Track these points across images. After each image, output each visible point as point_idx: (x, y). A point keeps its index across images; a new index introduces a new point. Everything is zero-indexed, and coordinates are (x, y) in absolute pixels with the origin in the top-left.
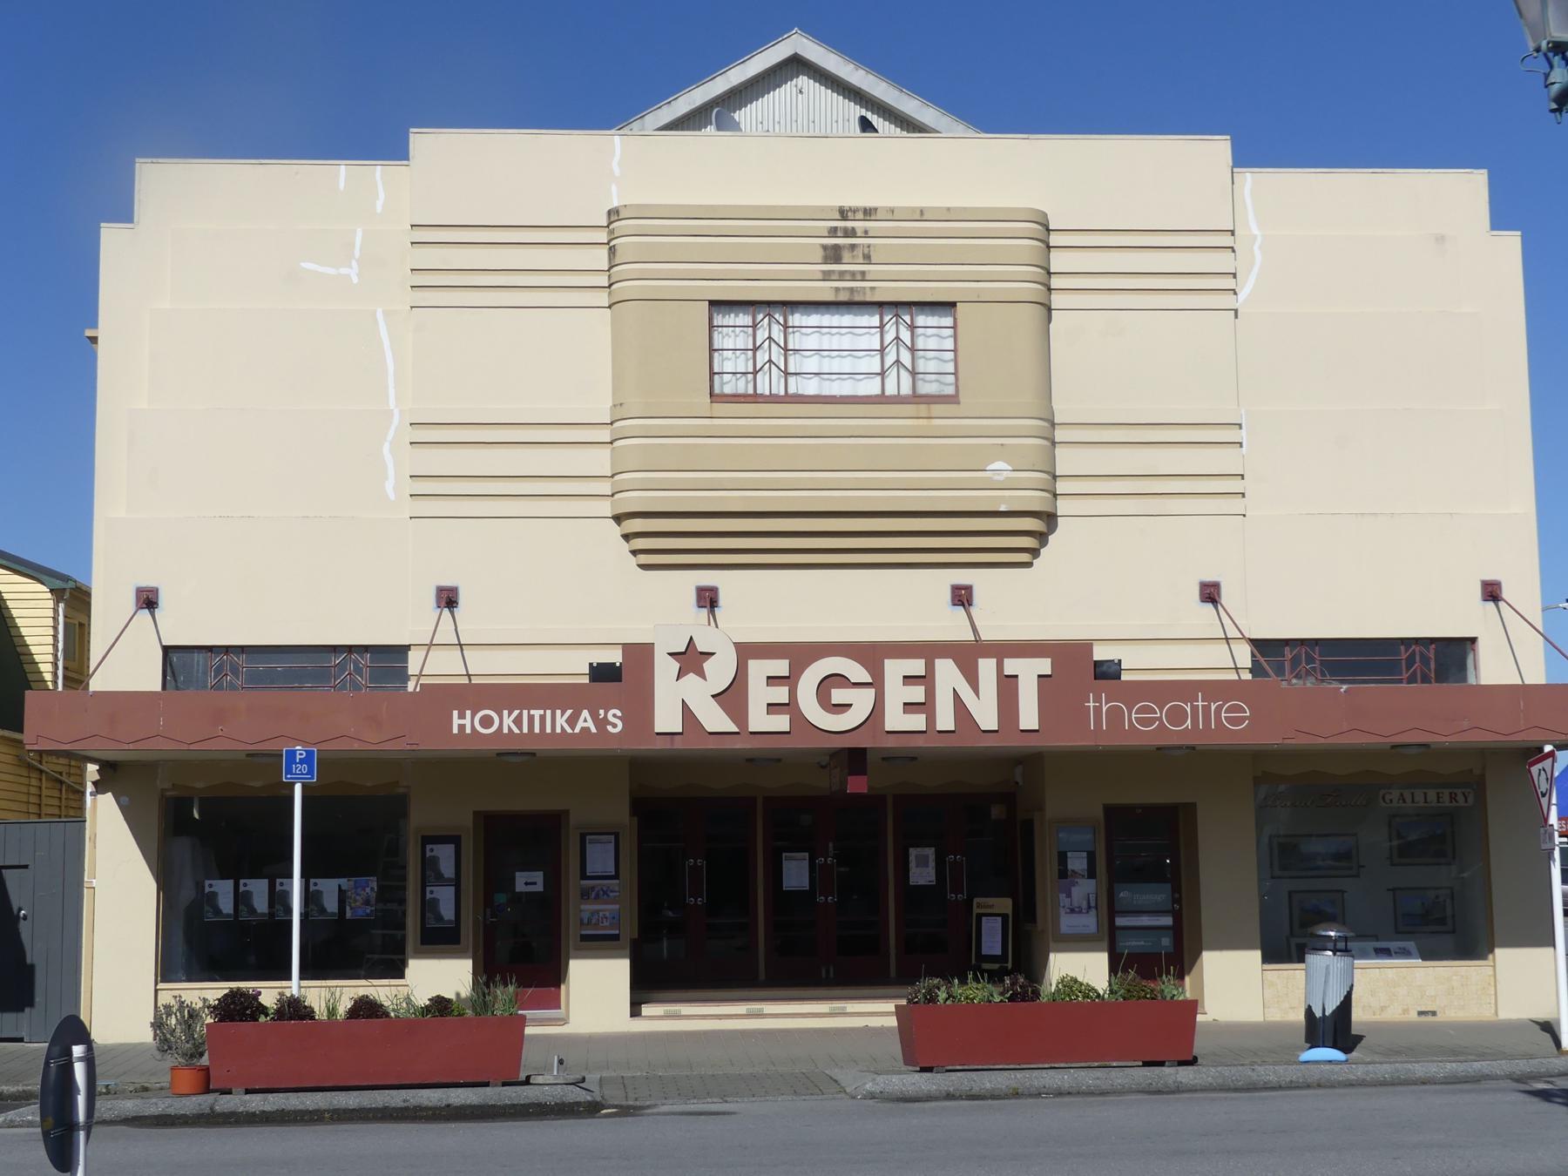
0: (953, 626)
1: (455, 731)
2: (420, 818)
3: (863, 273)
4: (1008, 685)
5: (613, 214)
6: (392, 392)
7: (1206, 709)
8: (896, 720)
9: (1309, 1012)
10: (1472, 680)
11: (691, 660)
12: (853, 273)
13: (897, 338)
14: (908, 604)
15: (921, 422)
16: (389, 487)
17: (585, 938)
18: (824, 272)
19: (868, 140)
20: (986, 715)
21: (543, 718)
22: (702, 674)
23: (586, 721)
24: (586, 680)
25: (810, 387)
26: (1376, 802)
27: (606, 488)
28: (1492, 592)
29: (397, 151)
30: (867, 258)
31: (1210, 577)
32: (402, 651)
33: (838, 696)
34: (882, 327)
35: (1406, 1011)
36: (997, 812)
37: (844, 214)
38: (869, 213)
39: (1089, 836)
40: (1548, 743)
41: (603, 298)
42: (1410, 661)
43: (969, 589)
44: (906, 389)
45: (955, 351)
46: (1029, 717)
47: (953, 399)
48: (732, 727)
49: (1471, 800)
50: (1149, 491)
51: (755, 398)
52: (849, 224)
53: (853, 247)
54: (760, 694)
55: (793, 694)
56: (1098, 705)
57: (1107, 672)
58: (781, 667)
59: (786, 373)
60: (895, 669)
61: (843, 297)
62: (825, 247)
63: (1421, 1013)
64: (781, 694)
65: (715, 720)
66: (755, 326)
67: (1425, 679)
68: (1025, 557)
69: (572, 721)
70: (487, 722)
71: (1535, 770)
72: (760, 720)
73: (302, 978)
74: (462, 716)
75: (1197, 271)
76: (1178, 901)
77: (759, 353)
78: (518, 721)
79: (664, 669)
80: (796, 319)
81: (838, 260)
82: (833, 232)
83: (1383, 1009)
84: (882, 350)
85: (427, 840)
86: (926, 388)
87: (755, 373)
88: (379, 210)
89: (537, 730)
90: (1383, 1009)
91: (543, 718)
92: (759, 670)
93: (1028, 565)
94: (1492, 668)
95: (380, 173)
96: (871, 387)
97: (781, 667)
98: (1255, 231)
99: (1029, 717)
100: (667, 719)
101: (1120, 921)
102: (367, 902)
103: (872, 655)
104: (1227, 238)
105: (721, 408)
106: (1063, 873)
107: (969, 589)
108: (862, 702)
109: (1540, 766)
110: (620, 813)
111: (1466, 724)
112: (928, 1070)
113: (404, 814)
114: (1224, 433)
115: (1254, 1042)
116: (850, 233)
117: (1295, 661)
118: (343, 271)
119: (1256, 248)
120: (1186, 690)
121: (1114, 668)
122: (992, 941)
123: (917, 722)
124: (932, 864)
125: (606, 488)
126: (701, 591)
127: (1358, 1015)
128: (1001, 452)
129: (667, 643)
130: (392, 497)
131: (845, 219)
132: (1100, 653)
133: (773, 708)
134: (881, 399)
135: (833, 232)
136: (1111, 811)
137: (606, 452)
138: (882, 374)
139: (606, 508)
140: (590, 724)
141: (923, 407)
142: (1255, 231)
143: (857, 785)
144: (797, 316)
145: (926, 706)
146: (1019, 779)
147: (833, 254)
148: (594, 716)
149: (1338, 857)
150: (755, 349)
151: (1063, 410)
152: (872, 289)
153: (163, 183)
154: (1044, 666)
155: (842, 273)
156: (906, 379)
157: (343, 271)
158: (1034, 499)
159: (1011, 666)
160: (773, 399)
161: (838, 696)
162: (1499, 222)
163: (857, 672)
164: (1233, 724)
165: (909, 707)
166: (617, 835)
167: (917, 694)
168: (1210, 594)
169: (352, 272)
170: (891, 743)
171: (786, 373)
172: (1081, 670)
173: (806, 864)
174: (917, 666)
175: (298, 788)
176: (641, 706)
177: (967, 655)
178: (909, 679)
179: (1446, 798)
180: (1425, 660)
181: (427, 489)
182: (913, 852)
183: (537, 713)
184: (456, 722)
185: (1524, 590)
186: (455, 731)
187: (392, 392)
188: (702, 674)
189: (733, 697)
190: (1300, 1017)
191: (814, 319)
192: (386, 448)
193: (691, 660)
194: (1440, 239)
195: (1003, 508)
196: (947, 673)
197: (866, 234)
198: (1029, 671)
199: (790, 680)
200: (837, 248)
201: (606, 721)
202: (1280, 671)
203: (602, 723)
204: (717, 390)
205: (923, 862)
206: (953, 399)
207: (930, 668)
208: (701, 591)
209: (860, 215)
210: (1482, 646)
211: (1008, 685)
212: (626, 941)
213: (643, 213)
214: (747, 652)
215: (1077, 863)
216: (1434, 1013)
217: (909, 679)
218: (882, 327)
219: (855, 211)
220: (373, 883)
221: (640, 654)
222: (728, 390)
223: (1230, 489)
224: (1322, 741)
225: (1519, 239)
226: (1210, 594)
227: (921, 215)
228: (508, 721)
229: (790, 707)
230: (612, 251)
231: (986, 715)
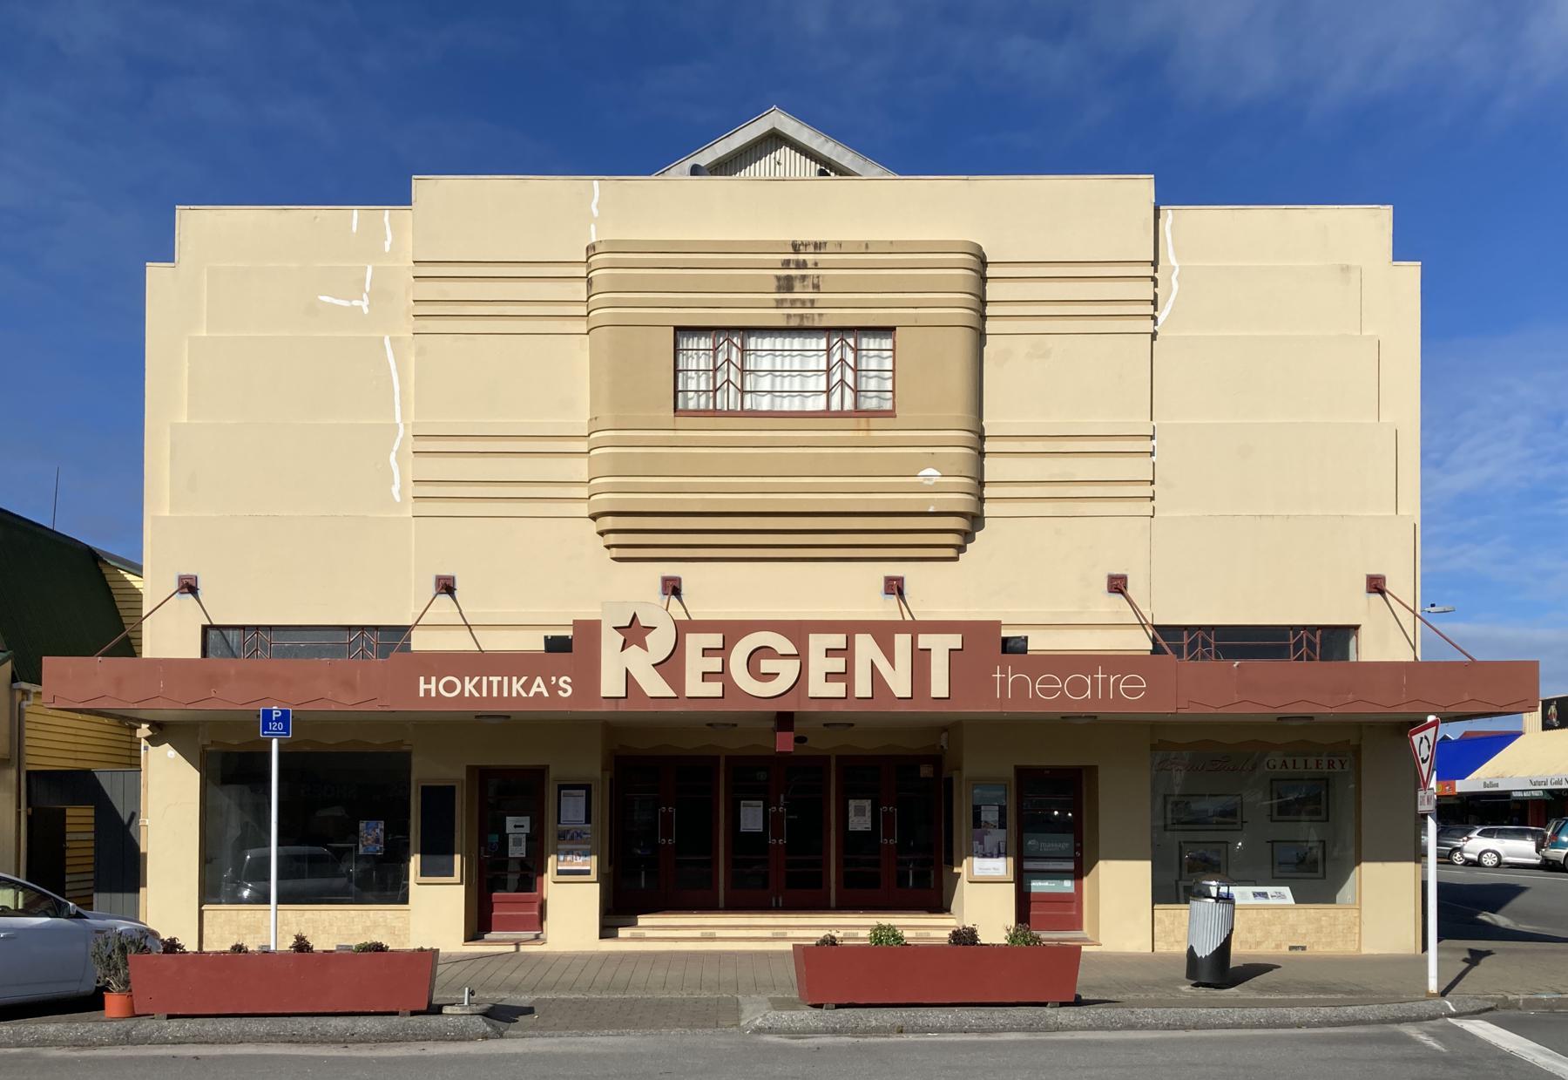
0: (887, 610)
1: (422, 694)
2: (426, 770)
3: (812, 301)
4: (921, 659)
5: (591, 249)
6: (397, 407)
7: (1106, 681)
8: (818, 687)
9: (1191, 950)
10: (1353, 658)
11: (634, 633)
12: (803, 301)
13: (842, 360)
14: (852, 590)
15: (861, 434)
16: (395, 489)
17: (560, 873)
20: (900, 683)
21: (500, 684)
22: (644, 647)
23: (539, 687)
25: (765, 404)
26: (1264, 760)
27: (583, 492)
28: (1376, 585)
29: (401, 197)
30: (816, 288)
31: (1117, 571)
32: (404, 630)
33: (767, 666)
34: (829, 350)
35: (1278, 946)
36: (926, 771)
37: (796, 247)
38: (818, 246)
39: (1001, 793)
41: (582, 327)
42: (1298, 645)
43: (901, 580)
44: (849, 405)
45: (893, 371)
46: (939, 686)
47: (890, 414)
49: (1347, 766)
50: (1063, 496)
51: (715, 413)
52: (801, 257)
53: (804, 277)
54: (695, 665)
55: (725, 664)
56: (1005, 676)
57: (1013, 647)
58: (715, 640)
59: (743, 392)
61: (794, 323)
62: (778, 278)
63: (1291, 948)
64: (715, 664)
65: (655, 686)
66: (715, 349)
67: (1310, 659)
68: (951, 552)
70: (450, 687)
71: (1416, 739)
72: (695, 687)
73: (279, 902)
74: (428, 682)
76: (1080, 849)
77: (719, 374)
78: (478, 687)
79: (610, 642)
80: (753, 343)
81: (790, 290)
82: (786, 264)
83: (1258, 944)
84: (829, 371)
85: (561, 787)
86: (870, 403)
87: (716, 390)
88: (387, 249)
89: (495, 694)
90: (1258, 944)
91: (500, 684)
92: (695, 642)
93: (956, 559)
94: (1371, 648)
95: (386, 215)
96: (819, 403)
97: (715, 640)
98: (1173, 262)
99: (939, 686)
100: (611, 685)
101: (1028, 865)
102: (377, 841)
103: (798, 631)
105: (682, 422)
106: (977, 821)
107: (901, 580)
108: (788, 672)
109: (1422, 734)
110: (592, 767)
111: (1350, 697)
112: (820, 1006)
115: (1135, 983)
116: (802, 265)
117: (1193, 646)
118: (356, 303)
119: (1174, 278)
122: (1553, 709)
123: (838, 689)
124: (868, 814)
125: (583, 492)
126: (665, 580)
128: (932, 461)
130: (398, 499)
131: (797, 251)
132: (1005, 633)
133: (707, 676)
134: (827, 413)
136: (1022, 773)
137: (584, 461)
138: (828, 392)
139: (584, 509)
140: (543, 689)
142: (1173, 262)
143: (784, 743)
144: (753, 340)
145: (847, 676)
146: (943, 743)
147: (786, 284)
149: (1224, 814)
150: (716, 370)
151: (990, 424)
152: (820, 315)
153: (197, 225)
154: (955, 641)
155: (793, 301)
157: (356, 303)
158: (961, 501)
159: (924, 641)
160: (730, 414)
161: (767, 666)
162: (1401, 252)
163: (784, 645)
164: (1131, 697)
166: (588, 788)
167: (838, 664)
168: (1117, 585)
170: (814, 707)
171: (743, 392)
172: (993, 646)
173: (760, 811)
174: (838, 641)
175: (275, 742)
176: (589, 674)
177: (883, 633)
178: (830, 652)
179: (1324, 764)
180: (1311, 645)
181: (427, 491)
182: (852, 803)
183: (495, 679)
184: (422, 686)
185: (1402, 584)
186: (422, 694)
187: (397, 407)
188: (644, 647)
189: (671, 666)
190: (1185, 950)
191: (767, 343)
192: (393, 456)
195: (931, 509)
196: (866, 647)
197: (816, 266)
198: (940, 646)
199: (724, 651)
200: (789, 278)
202: (1178, 651)
203: (554, 689)
204: (680, 406)
205: (860, 811)
206: (890, 414)
207: (850, 642)
208: (665, 580)
209: (811, 249)
210: (1362, 632)
211: (921, 659)
212: (593, 876)
213: (616, 247)
214: (683, 628)
215: (990, 815)
216: (1304, 948)
217: (830, 652)
218: (829, 350)
219: (806, 245)
220: (381, 825)
221: (589, 630)
222: (692, 405)
223: (1148, 491)
224: (1213, 711)
226: (1117, 585)
227: (866, 247)
228: (469, 686)
229: (723, 674)
230: (590, 282)
231: (900, 683)
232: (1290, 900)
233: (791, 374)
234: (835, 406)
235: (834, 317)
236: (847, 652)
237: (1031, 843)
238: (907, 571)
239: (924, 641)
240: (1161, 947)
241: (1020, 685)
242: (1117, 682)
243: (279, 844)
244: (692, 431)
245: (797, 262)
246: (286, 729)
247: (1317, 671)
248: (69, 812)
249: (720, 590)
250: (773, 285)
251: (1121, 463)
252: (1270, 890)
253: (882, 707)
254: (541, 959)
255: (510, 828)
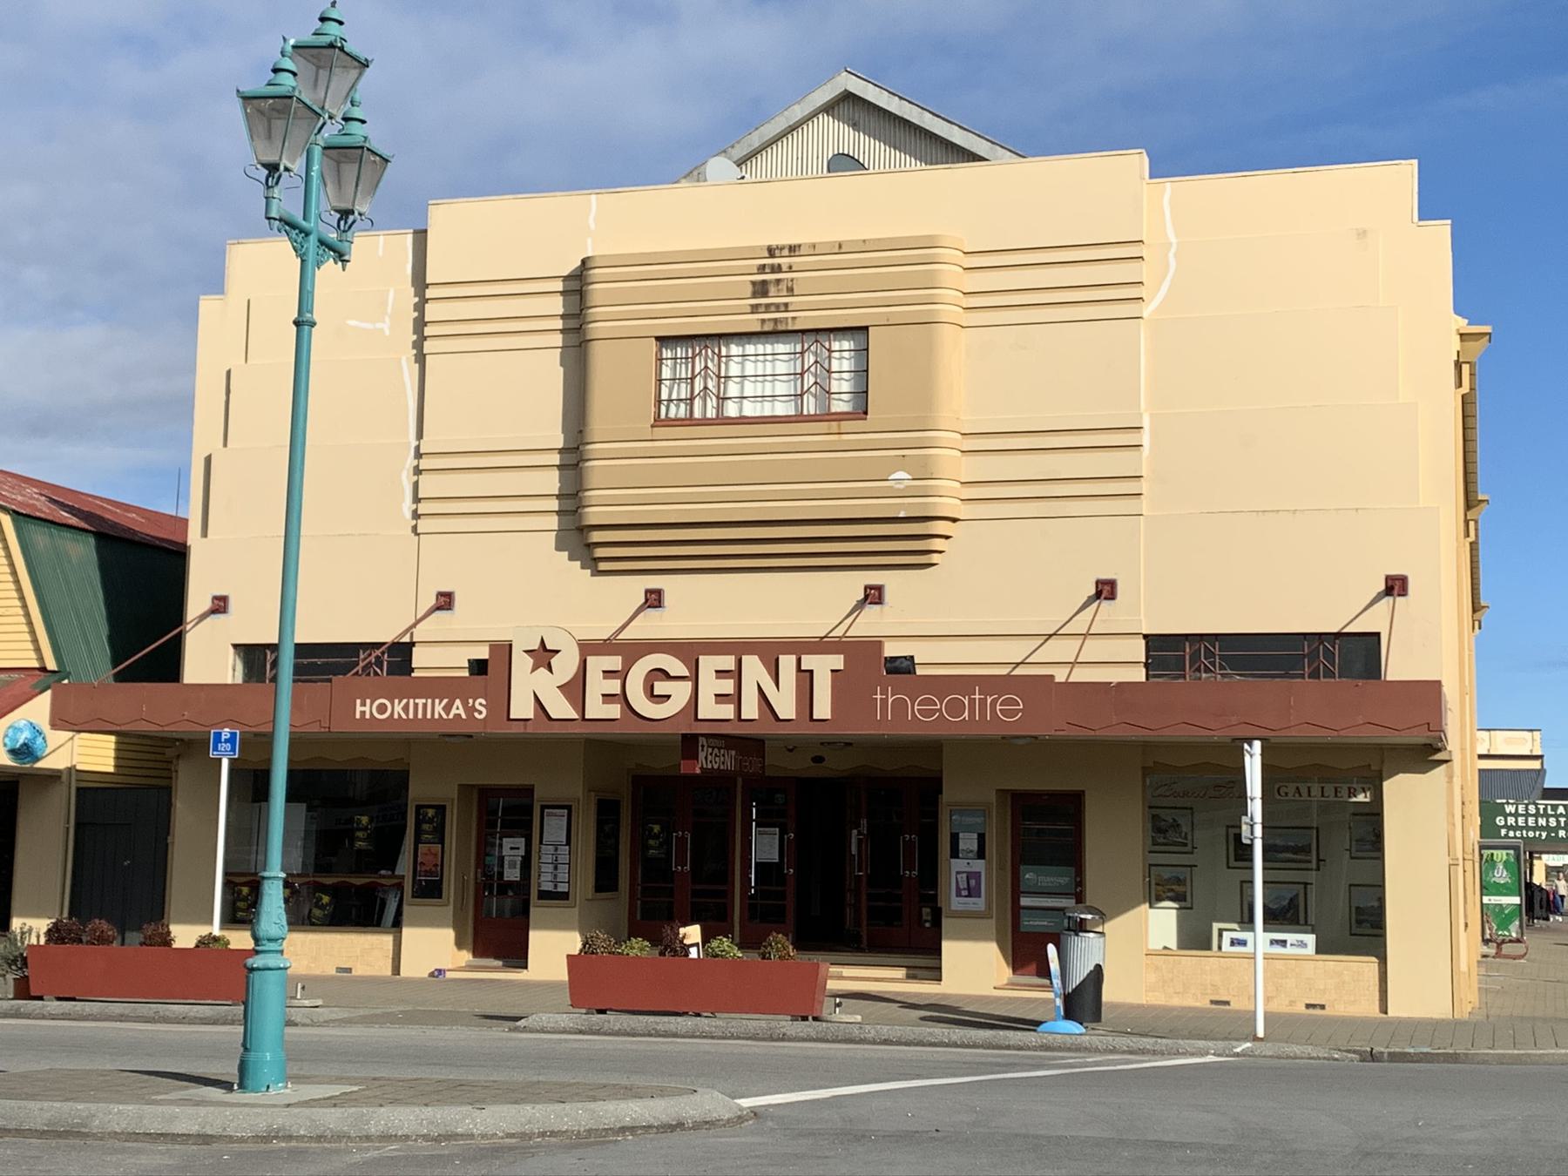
2: (419, 791)
3: (786, 305)
4: (806, 678)
7: (983, 702)
8: (709, 709)
11: (543, 656)
12: (777, 306)
14: (811, 604)
18: (752, 306)
19: (847, 182)
20: (786, 706)
21: (425, 705)
23: (458, 709)
24: (466, 674)
25: (750, 410)
33: (661, 687)
35: (1292, 1003)
37: (771, 252)
38: (793, 249)
40: (224, 724)
46: (823, 708)
48: (574, 715)
50: (1047, 494)
53: (778, 281)
54: (597, 686)
56: (886, 698)
57: (902, 667)
58: (615, 662)
60: (708, 664)
61: (768, 327)
62: (754, 283)
63: (1308, 1006)
64: (614, 686)
65: (560, 708)
69: (447, 709)
70: (382, 709)
72: (596, 709)
74: (363, 704)
75: (1097, 282)
78: (406, 709)
81: (765, 294)
82: (762, 269)
91: (425, 705)
92: (597, 664)
96: (783, 409)
97: (615, 662)
99: (823, 708)
100: (521, 708)
101: (1025, 901)
104: (1129, 250)
105: (661, 432)
108: (680, 694)
110: (572, 787)
111: (1234, 720)
113: (404, 785)
114: (1124, 438)
116: (777, 269)
117: (1195, 657)
118: (379, 325)
119: (1171, 255)
120: (965, 684)
121: (906, 663)
123: (728, 711)
126: (648, 592)
127: (1108, 995)
129: (523, 642)
132: (890, 650)
133: (608, 698)
134: (799, 418)
135: (762, 269)
140: (461, 712)
141: (834, 424)
142: (1173, 240)
147: (761, 289)
148: (465, 704)
152: (794, 318)
154: (838, 662)
155: (767, 306)
156: (712, 403)
157: (379, 325)
159: (809, 662)
161: (661, 687)
163: (676, 667)
165: (721, 698)
166: (569, 808)
167: (728, 686)
169: (385, 326)
174: (728, 662)
178: (721, 673)
183: (420, 702)
184: (359, 709)
189: (576, 689)
193: (543, 656)
194: (1362, 234)
196: (754, 668)
198: (823, 666)
199: (622, 675)
200: (764, 282)
201: (474, 709)
203: (470, 710)
208: (648, 592)
209: (786, 252)
211: (806, 678)
214: (588, 649)
216: (1323, 1007)
217: (721, 673)
219: (782, 249)
221: (504, 650)
223: (1126, 487)
225: (1448, 229)
228: (398, 708)
231: (786, 706)
232: (1311, 949)
233: (761, 379)
234: (697, 414)
235: (806, 320)
236: (737, 674)
237: (1029, 876)
238: (197, 601)
239: (809, 662)
240: (1398, 1008)
241: (900, 706)
242: (994, 702)
243: (1265, 860)
244: (672, 441)
245: (772, 266)
246: (233, 750)
247: (1340, 687)
248: (1139, 675)
249: (704, 605)
250: (749, 289)
251: (1083, 466)
252: (1291, 937)
253: (772, 729)
254: (527, 985)
255: (506, 851)
